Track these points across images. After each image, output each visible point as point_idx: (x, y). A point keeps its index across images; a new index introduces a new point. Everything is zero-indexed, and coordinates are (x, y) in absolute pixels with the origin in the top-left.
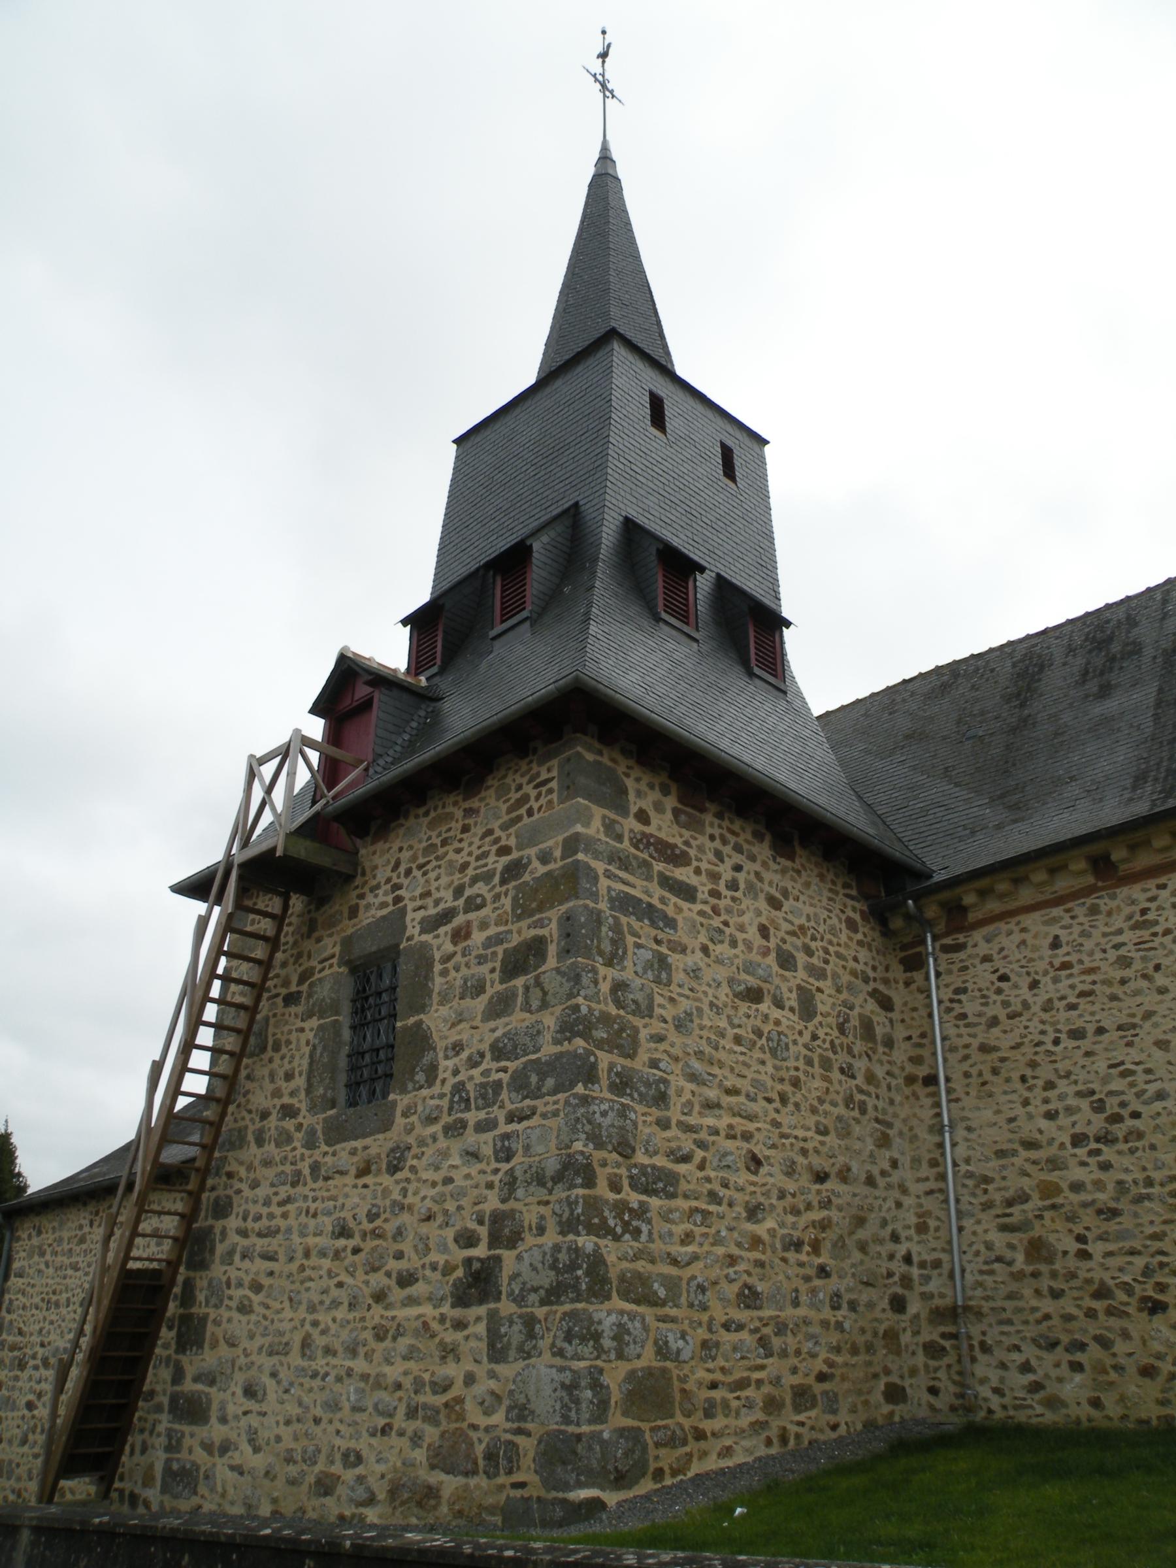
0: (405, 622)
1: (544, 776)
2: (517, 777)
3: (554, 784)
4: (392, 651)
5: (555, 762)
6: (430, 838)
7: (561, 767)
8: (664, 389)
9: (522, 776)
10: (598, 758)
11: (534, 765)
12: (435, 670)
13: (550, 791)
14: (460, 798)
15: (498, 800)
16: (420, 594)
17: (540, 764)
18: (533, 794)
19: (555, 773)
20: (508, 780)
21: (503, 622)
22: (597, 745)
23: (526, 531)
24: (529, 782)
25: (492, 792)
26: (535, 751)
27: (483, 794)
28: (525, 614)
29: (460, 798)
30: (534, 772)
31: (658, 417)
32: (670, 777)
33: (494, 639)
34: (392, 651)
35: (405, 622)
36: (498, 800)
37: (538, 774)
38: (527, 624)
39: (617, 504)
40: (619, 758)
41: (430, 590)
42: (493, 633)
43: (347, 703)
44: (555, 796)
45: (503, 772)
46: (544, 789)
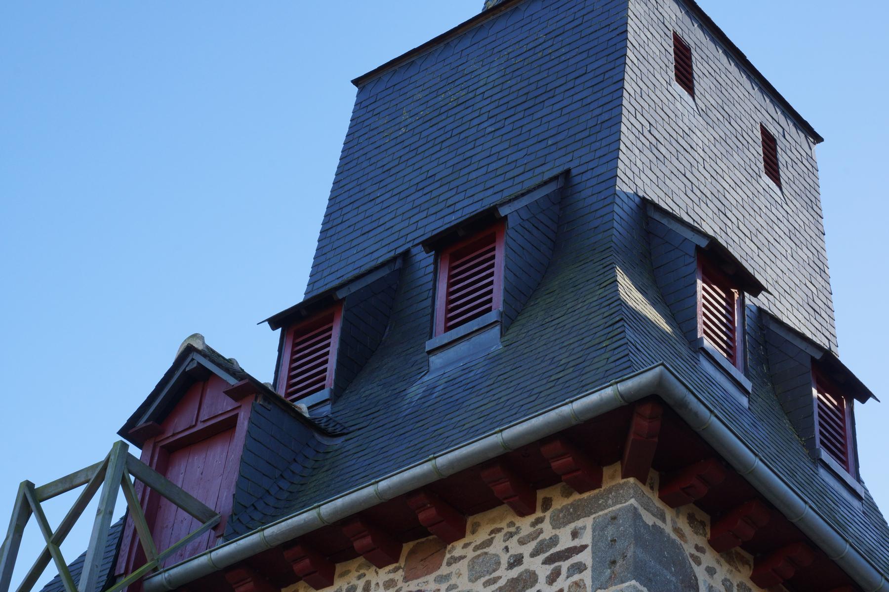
0: (275, 322)
1: (565, 542)
2: (513, 543)
3: (585, 557)
4: (259, 356)
5: (587, 522)
6: (517, 560)
7: (598, 529)
8: (695, 36)
9: (522, 542)
10: (659, 523)
11: (546, 526)
12: (324, 394)
13: (579, 568)
14: (399, 576)
15: (473, 579)
16: (293, 292)
17: (557, 523)
18: (543, 572)
19: (586, 538)
20: (496, 548)
21: (448, 329)
22: (658, 503)
23: (496, 199)
24: (533, 555)
25: (462, 566)
26: (547, 504)
27: (444, 570)
28: (492, 317)
29: (399, 576)
30: (546, 535)
31: (685, 75)
32: (753, 578)
33: (430, 352)
34: (259, 356)
35: (275, 322)
36: (473, 579)
37: (554, 541)
38: (497, 330)
39: (639, 173)
40: (687, 529)
41: (304, 288)
42: (429, 345)
43: (182, 424)
44: (587, 577)
45: (482, 535)
46: (565, 565)
